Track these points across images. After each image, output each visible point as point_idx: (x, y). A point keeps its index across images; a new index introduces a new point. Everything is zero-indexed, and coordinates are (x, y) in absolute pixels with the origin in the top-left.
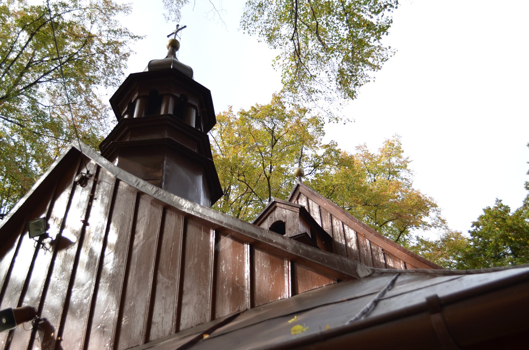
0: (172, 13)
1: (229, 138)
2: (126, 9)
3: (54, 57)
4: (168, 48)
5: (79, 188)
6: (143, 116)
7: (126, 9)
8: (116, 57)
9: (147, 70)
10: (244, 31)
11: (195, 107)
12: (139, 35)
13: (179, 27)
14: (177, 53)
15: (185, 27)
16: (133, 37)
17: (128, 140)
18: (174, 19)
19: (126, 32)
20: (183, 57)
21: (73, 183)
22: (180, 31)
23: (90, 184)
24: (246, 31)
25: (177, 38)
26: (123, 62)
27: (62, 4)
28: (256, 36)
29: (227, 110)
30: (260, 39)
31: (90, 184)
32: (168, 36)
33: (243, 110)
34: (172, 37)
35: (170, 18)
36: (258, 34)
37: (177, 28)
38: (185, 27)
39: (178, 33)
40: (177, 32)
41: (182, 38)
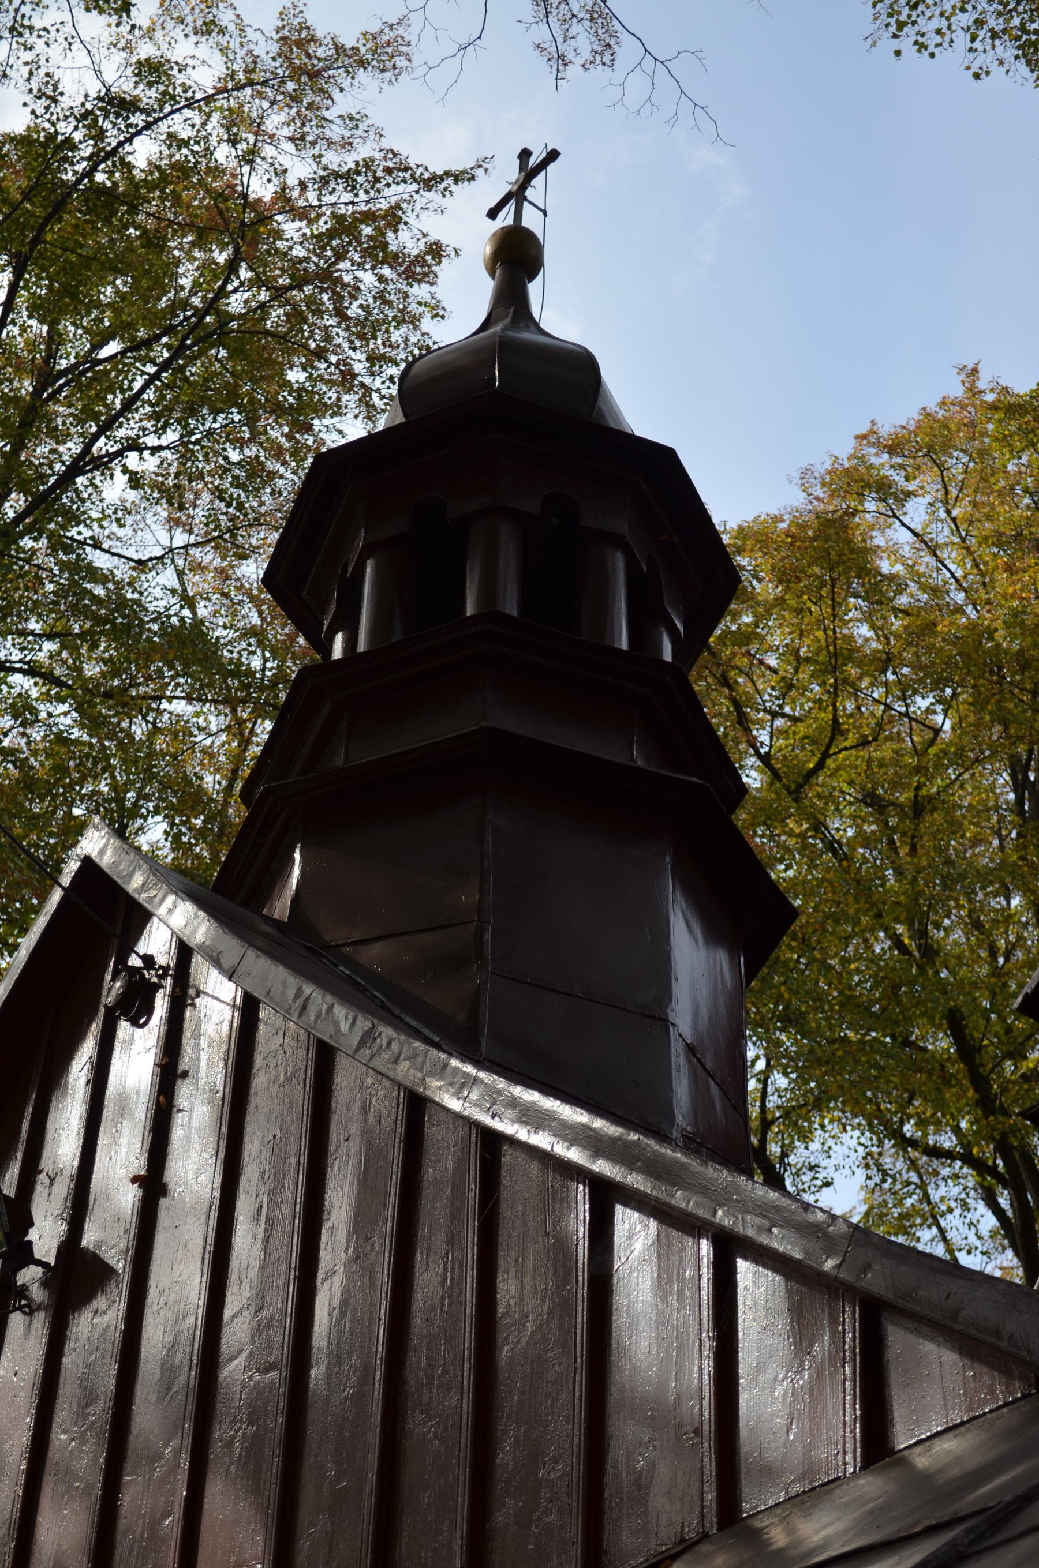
0: (576, 28)
1: (989, 518)
2: (380, 53)
3: (142, 334)
4: (492, 275)
5: (124, 1028)
6: (398, 636)
7: (380, 53)
8: (381, 279)
9: (400, 419)
10: (895, 44)
11: (618, 541)
12: (455, 167)
13: (533, 161)
14: (534, 288)
15: (553, 155)
16: (430, 182)
17: (340, 760)
18: (587, 55)
19: (400, 169)
20: (558, 311)
21: (102, 1010)
22: (538, 181)
23: (161, 1004)
24: (906, 44)
25: (531, 220)
26: (420, 291)
27: (111, 102)
28: (955, 55)
29: (957, 390)
30: (981, 60)
31: (161, 1004)
32: (493, 214)
33: (1005, 389)
34: (506, 218)
35: (570, 55)
36: (962, 40)
37: (523, 167)
38: (553, 155)
39: (529, 193)
40: (525, 184)
41: (554, 216)
